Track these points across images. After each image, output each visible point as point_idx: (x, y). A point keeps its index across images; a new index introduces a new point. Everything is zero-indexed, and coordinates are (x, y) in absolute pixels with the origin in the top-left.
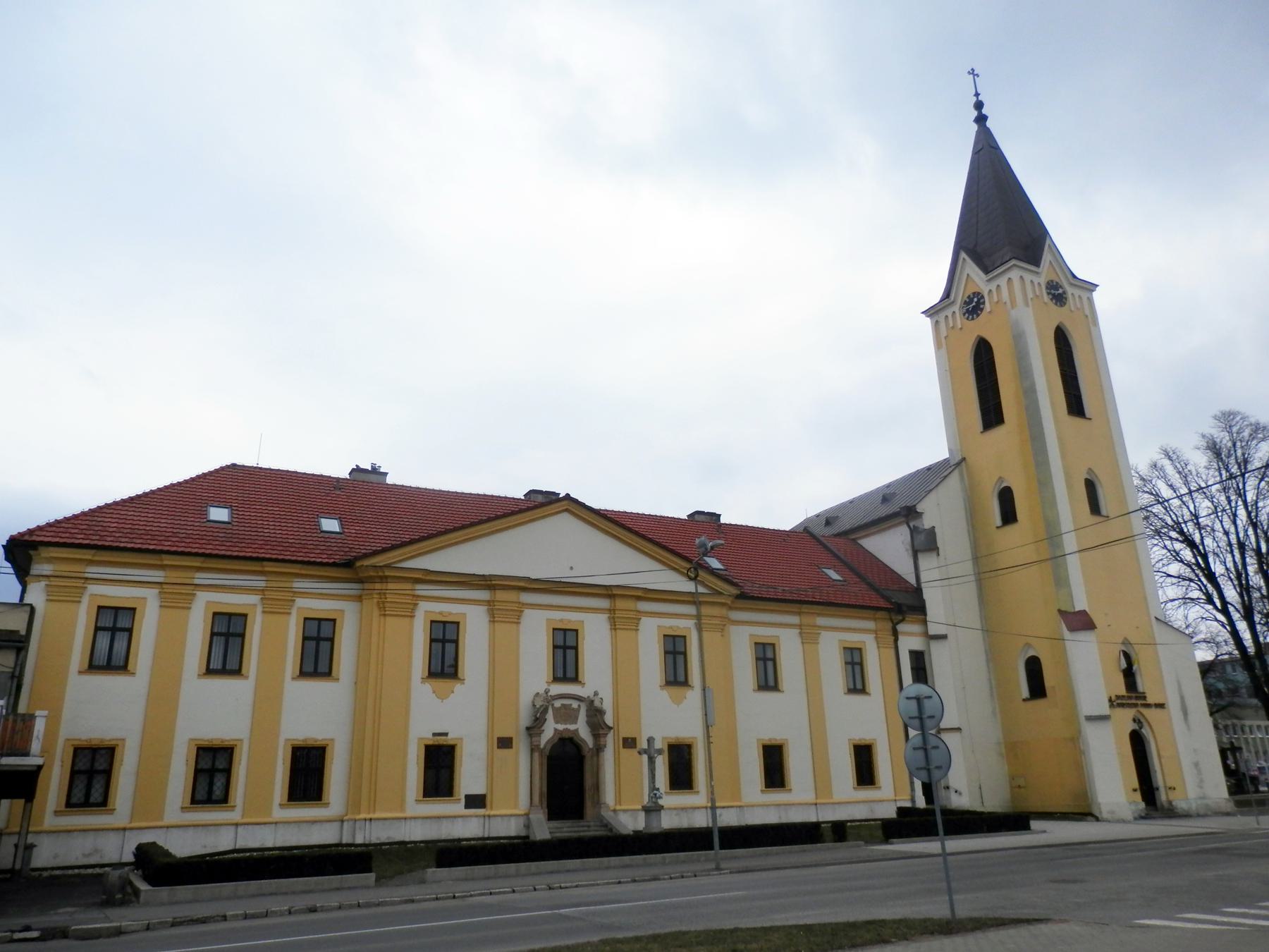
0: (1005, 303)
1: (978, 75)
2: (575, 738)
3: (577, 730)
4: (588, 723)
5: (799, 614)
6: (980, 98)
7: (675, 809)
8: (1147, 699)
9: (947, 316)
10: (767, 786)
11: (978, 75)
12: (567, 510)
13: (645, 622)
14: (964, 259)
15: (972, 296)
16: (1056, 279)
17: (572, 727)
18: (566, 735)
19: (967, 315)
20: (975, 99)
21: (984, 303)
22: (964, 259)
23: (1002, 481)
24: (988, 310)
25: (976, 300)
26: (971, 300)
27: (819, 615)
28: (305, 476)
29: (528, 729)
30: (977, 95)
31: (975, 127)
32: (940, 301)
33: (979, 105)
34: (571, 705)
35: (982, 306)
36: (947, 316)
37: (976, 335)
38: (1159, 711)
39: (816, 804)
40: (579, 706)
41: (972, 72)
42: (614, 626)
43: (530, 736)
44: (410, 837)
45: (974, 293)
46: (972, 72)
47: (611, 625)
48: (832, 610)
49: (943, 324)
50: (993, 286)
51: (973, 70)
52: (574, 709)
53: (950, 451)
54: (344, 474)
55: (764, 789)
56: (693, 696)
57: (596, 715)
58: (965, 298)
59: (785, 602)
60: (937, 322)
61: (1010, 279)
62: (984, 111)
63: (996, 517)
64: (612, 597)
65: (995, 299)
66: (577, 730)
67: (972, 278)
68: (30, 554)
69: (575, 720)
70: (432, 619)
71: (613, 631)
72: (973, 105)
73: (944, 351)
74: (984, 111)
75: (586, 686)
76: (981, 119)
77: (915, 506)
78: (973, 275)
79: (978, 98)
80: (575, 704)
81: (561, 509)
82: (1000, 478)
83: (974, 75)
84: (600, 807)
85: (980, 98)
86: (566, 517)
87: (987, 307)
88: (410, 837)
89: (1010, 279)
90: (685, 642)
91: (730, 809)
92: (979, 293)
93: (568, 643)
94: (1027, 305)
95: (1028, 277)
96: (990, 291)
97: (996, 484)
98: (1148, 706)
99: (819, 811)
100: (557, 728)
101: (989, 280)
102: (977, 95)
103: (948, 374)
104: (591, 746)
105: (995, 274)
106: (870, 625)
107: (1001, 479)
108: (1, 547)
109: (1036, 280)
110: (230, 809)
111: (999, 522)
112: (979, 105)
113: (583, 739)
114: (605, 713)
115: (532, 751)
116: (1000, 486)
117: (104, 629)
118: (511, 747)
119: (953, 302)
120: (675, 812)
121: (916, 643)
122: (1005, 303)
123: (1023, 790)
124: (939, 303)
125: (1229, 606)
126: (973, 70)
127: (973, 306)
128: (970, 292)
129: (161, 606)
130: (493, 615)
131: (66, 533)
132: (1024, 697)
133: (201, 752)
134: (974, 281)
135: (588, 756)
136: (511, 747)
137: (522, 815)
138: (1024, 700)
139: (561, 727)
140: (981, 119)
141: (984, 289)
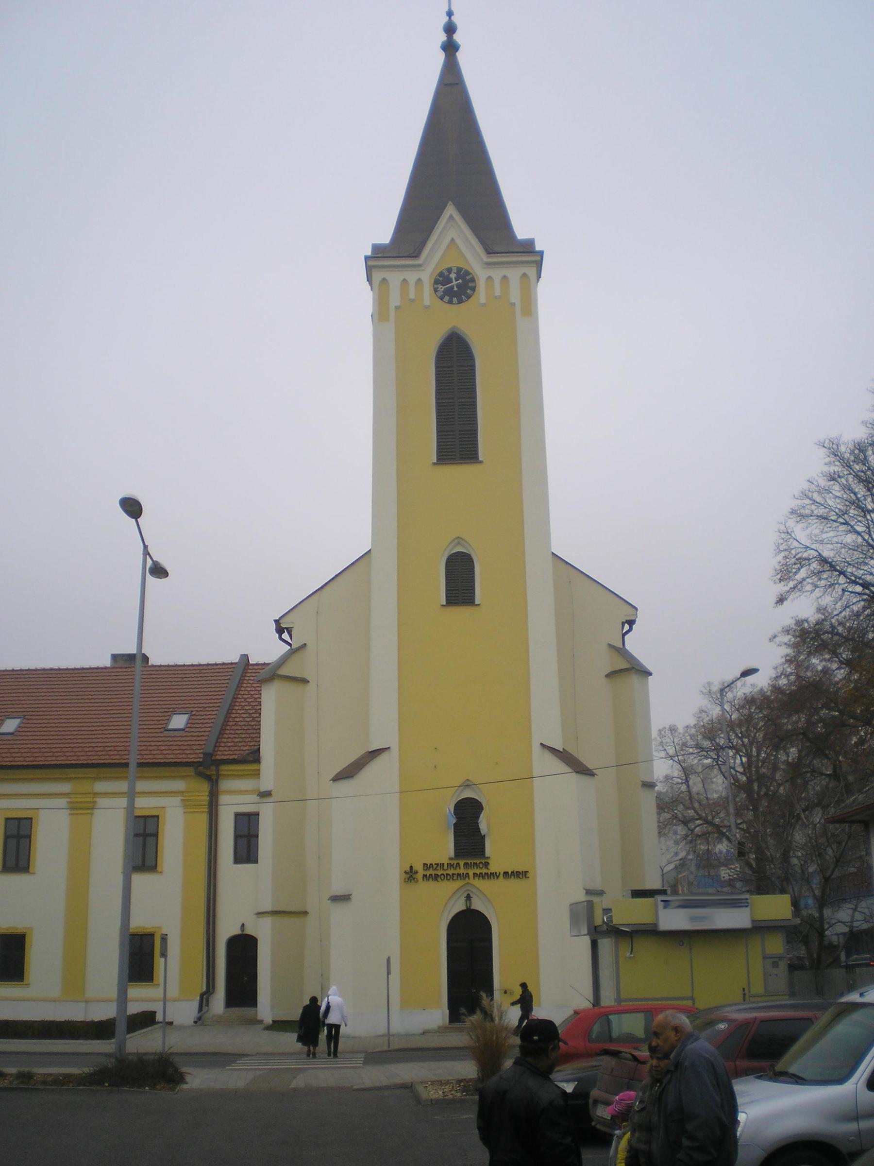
6: (453, 18)
8: (489, 867)
14: (453, 240)
21: (474, 289)
22: (453, 240)
24: (483, 300)
27: (96, 779)
28: (67, 672)
30: (450, 14)
31: (441, 57)
33: (450, 29)
35: (455, 300)
37: (450, 326)
38: (513, 883)
48: (38, 773)
50: (497, 274)
54: (107, 662)
59: (72, 768)
70: (7, 817)
76: (450, 48)
79: (450, 17)
87: (481, 294)
89: (405, 280)
90: (158, 821)
93: (148, 831)
96: (419, 280)
98: (493, 875)
101: (489, 264)
102: (450, 14)
106: (179, 785)
109: (412, 277)
112: (450, 29)
117: (241, 836)
121: (246, 804)
126: (411, 867)
129: (184, 812)
133: (606, 945)
140: (450, 48)
141: (481, 274)
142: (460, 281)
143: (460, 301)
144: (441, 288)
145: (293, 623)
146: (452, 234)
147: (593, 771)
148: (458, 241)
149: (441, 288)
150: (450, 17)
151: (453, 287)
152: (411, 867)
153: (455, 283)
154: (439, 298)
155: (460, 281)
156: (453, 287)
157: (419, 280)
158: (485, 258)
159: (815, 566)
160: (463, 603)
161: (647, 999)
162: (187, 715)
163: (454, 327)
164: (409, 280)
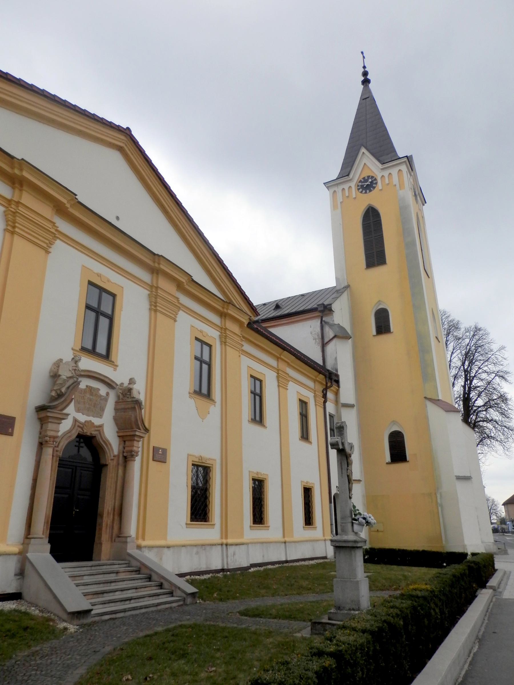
0: (395, 185)
2: (98, 438)
3: (101, 426)
4: (115, 419)
5: (278, 359)
7: (196, 546)
9: (343, 189)
10: (192, 520)
12: (120, 149)
13: (182, 316)
14: (363, 153)
15: (366, 178)
17: (97, 421)
18: (88, 431)
19: (361, 190)
21: (376, 183)
22: (363, 153)
23: (380, 304)
24: (380, 188)
25: (370, 180)
26: (366, 181)
29: (40, 409)
30: (364, 67)
32: (337, 179)
33: (365, 74)
34: (99, 390)
35: (374, 185)
36: (343, 189)
37: (367, 204)
39: (285, 543)
40: (108, 394)
42: (154, 308)
43: (43, 421)
45: (368, 177)
46: (362, 53)
47: (151, 305)
49: (339, 194)
50: (386, 173)
52: (101, 396)
53: (337, 279)
55: (189, 522)
56: (215, 410)
57: (134, 408)
58: (361, 178)
60: (335, 191)
61: (390, 173)
62: (369, 77)
63: (373, 329)
64: (154, 271)
65: (387, 181)
66: (101, 426)
67: (367, 165)
69: (100, 414)
71: (153, 312)
72: (362, 72)
73: (339, 211)
74: (369, 77)
75: (118, 368)
76: (366, 82)
77: (331, 304)
78: (369, 164)
80: (103, 390)
82: (379, 301)
84: (126, 542)
85: (366, 69)
86: (116, 157)
87: (379, 186)
89: (390, 173)
91: (241, 546)
92: (372, 177)
96: (383, 176)
97: (375, 305)
99: (35, 536)
100: (69, 416)
101: (382, 169)
102: (364, 67)
103: (341, 226)
104: (116, 452)
105: (386, 166)
107: (379, 302)
109: (346, 186)
110: (266, 528)
111: (374, 332)
112: (365, 74)
113: (108, 441)
115: (41, 445)
116: (379, 306)
118: (11, 434)
119: (351, 180)
120: (195, 549)
122: (395, 185)
123: (380, 534)
124: (336, 179)
127: (368, 185)
128: (365, 174)
130: (14, 222)
132: (387, 462)
134: (369, 168)
135: (111, 464)
136: (11, 434)
137: (15, 554)
138: (387, 463)
139: (82, 418)
140: (366, 82)
141: (378, 175)
143: (370, 191)
146: (365, 160)
154: (86, 304)
157: (350, 187)
159: (455, 367)
160: (385, 332)
163: (369, 204)
164: (402, 169)
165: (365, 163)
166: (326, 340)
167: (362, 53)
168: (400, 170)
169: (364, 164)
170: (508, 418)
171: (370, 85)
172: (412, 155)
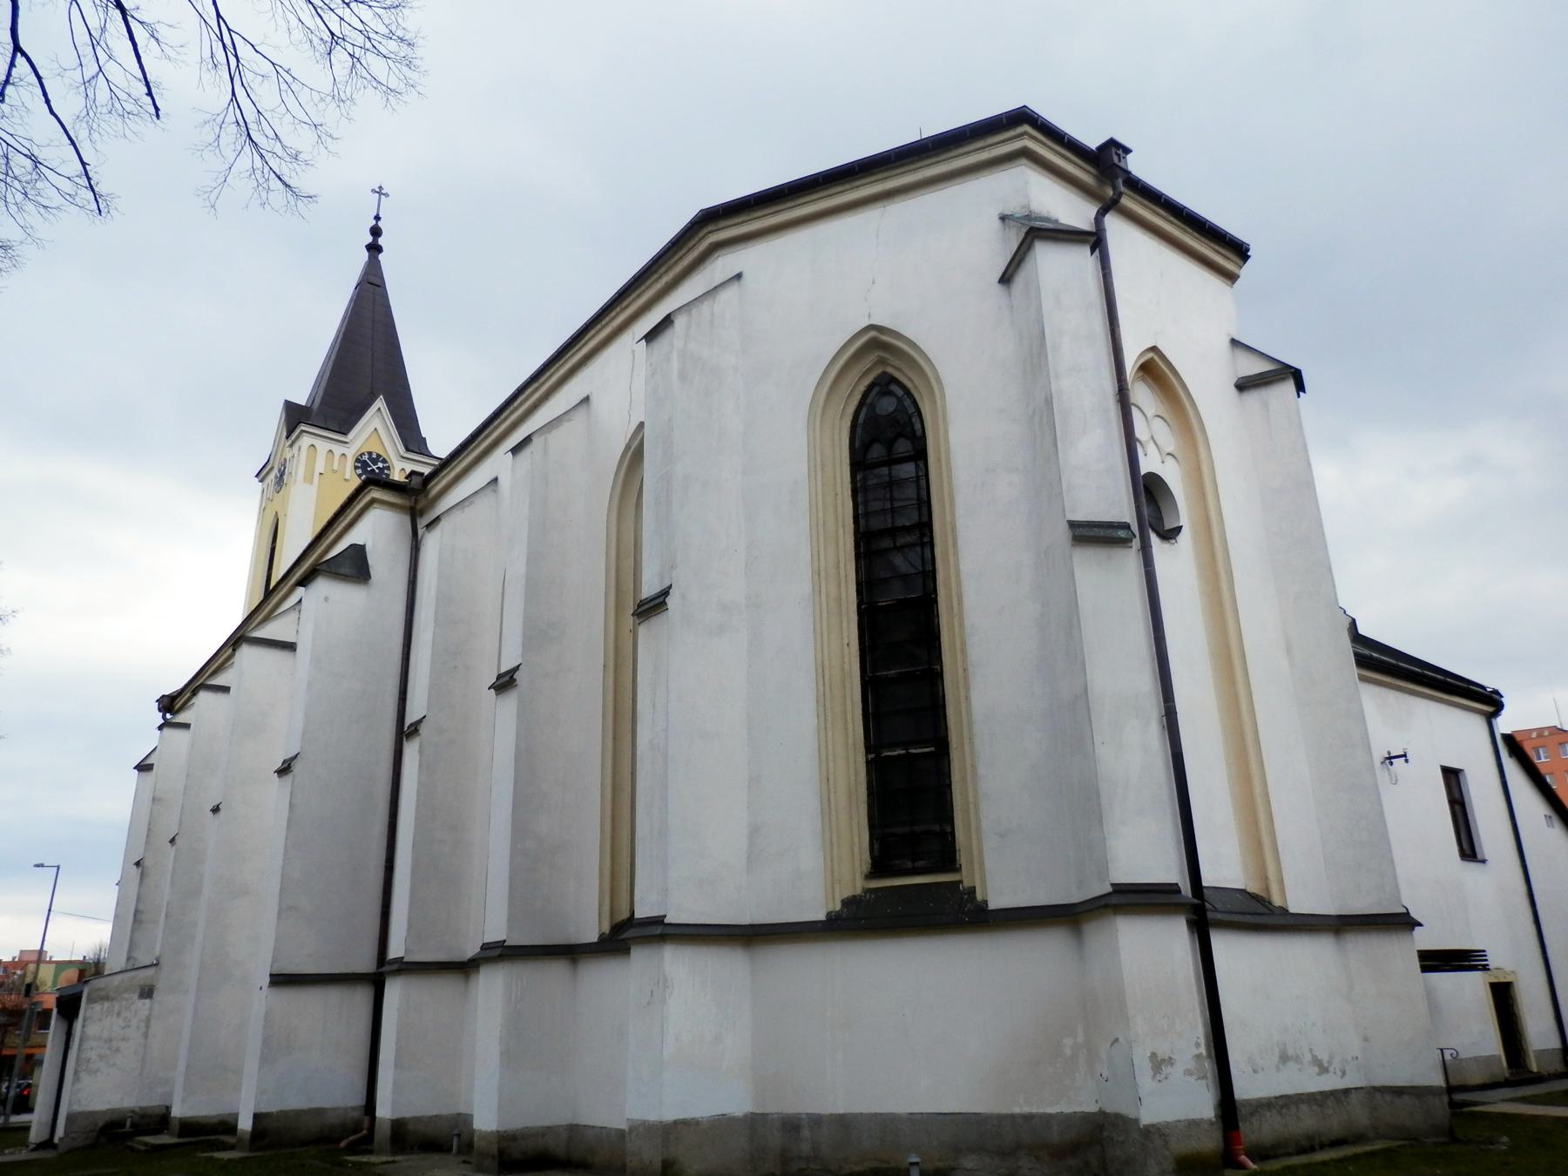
1: (387, 195)
6: (379, 223)
11: (387, 195)
14: (379, 409)
16: (376, 449)
20: (374, 222)
22: (379, 409)
30: (377, 218)
31: (365, 255)
33: (376, 232)
41: (380, 191)
44: (1265, 406)
46: (124, 214)
51: (380, 187)
62: (381, 241)
68: (1196, 915)
74: (381, 241)
76: (374, 249)
79: (377, 222)
81: (826, 657)
83: (380, 193)
88: (1265, 406)
94: (309, 479)
95: (323, 446)
102: (377, 218)
108: (1307, 391)
109: (338, 450)
112: (376, 232)
114: (1248, 250)
125: (1138, 444)
126: (380, 187)
131: (842, 488)
140: (374, 249)
142: (377, 471)
144: (366, 457)
145: (1484, 951)
147: (1133, 407)
148: (382, 408)
149: (366, 457)
150: (377, 222)
151: (370, 466)
152: (374, 191)
153: (374, 467)
155: (377, 471)
156: (370, 466)
158: (402, 449)
161: (1245, 670)
162: (1079, 574)
165: (495, 480)
166: (267, 631)
167: (124, 214)
168: (344, 454)
169: (373, 429)
170: (101, 950)
171: (381, 257)
172: (286, 401)
